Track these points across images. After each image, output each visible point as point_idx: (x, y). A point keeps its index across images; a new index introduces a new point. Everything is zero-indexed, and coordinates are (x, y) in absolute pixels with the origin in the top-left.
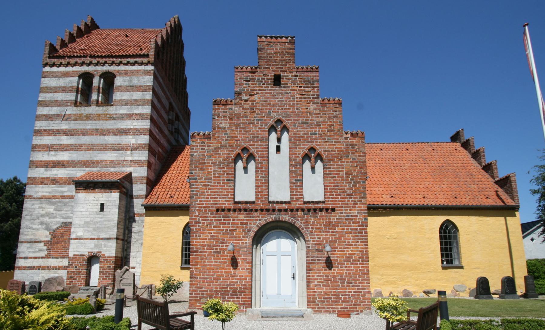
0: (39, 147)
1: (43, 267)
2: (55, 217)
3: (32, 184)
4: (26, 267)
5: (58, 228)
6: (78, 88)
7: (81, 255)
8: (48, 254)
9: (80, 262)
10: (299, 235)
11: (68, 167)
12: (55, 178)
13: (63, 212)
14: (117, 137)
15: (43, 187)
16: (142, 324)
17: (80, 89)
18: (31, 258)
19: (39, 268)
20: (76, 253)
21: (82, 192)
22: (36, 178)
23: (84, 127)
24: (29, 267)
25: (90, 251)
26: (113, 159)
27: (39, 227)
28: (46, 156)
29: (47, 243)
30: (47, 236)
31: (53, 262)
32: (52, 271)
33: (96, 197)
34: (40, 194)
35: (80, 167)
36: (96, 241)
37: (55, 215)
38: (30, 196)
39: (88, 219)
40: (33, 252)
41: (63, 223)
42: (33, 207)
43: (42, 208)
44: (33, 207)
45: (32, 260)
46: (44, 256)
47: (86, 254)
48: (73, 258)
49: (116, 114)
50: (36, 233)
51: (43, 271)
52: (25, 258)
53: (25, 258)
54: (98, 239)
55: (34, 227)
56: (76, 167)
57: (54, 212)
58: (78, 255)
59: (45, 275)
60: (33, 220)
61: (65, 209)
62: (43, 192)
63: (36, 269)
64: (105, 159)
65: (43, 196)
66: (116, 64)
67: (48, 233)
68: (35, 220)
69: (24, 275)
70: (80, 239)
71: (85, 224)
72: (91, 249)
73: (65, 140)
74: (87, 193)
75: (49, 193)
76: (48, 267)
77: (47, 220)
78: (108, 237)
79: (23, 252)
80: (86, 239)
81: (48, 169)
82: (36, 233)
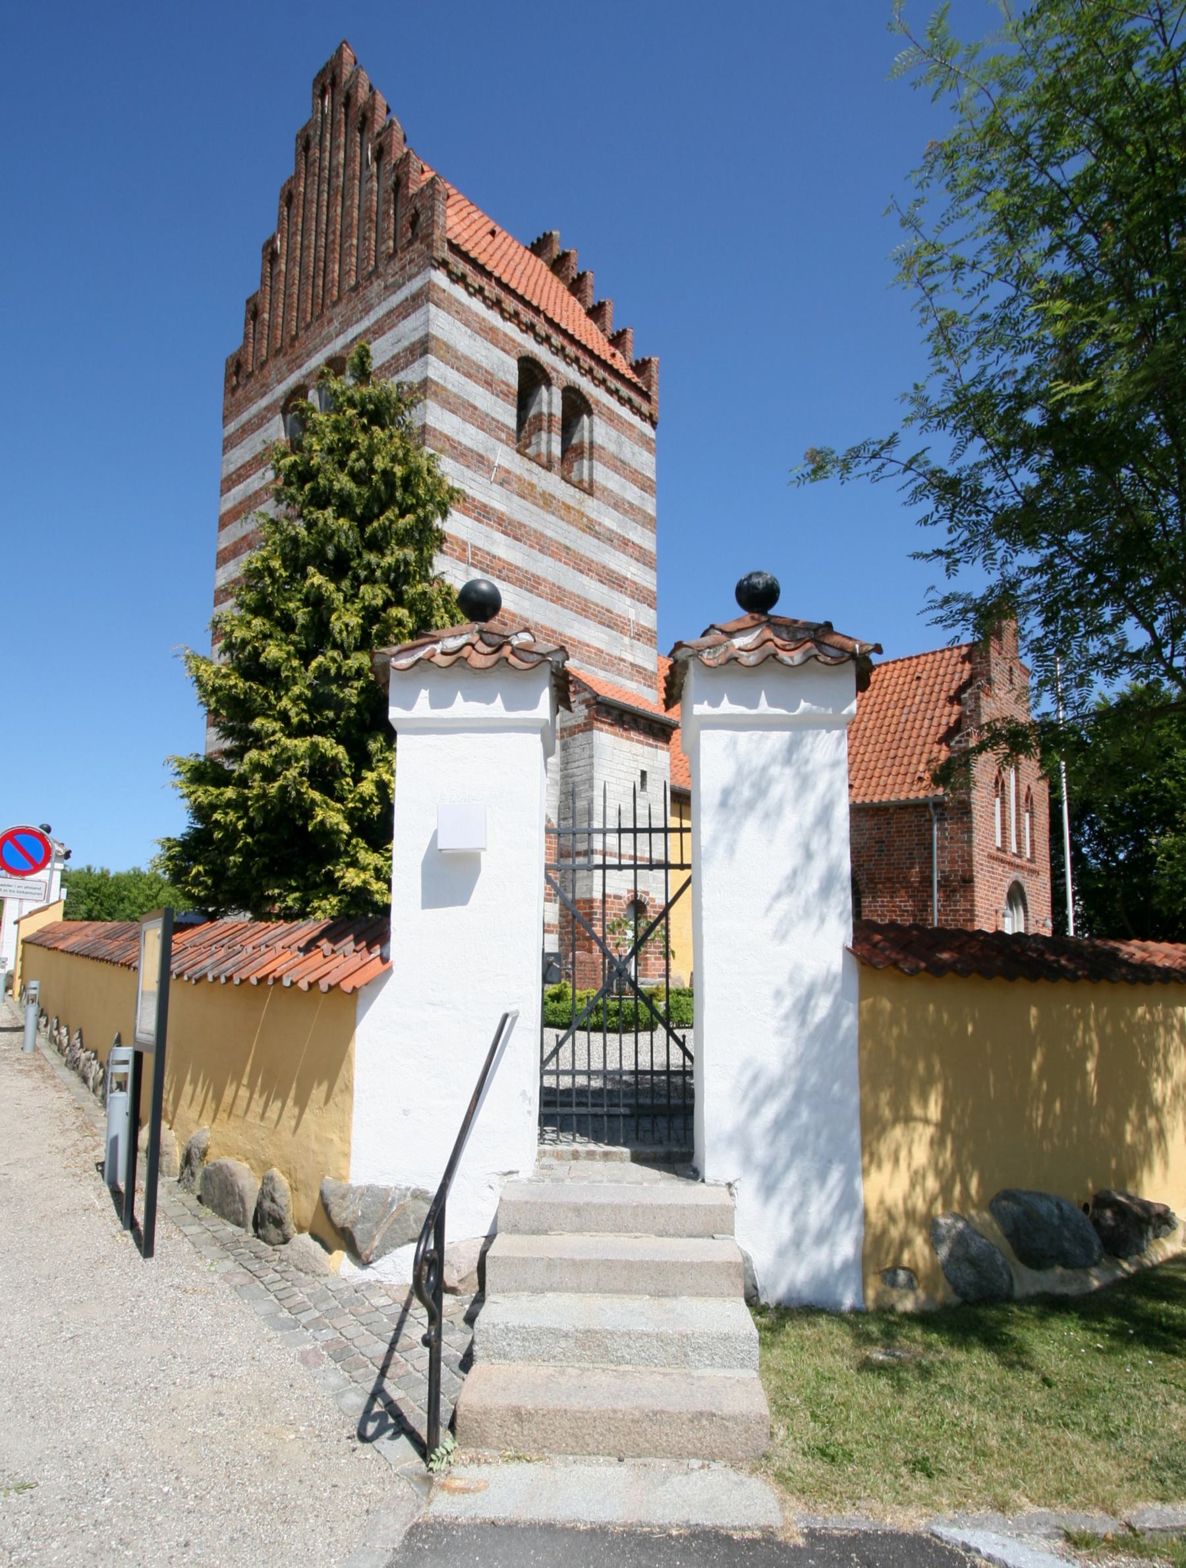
6: (591, 459)
10: (1020, 901)
17: (586, 455)
21: (607, 731)
23: (540, 528)
26: (602, 646)
49: (600, 524)
64: (587, 639)
66: (580, 367)
74: (616, 734)
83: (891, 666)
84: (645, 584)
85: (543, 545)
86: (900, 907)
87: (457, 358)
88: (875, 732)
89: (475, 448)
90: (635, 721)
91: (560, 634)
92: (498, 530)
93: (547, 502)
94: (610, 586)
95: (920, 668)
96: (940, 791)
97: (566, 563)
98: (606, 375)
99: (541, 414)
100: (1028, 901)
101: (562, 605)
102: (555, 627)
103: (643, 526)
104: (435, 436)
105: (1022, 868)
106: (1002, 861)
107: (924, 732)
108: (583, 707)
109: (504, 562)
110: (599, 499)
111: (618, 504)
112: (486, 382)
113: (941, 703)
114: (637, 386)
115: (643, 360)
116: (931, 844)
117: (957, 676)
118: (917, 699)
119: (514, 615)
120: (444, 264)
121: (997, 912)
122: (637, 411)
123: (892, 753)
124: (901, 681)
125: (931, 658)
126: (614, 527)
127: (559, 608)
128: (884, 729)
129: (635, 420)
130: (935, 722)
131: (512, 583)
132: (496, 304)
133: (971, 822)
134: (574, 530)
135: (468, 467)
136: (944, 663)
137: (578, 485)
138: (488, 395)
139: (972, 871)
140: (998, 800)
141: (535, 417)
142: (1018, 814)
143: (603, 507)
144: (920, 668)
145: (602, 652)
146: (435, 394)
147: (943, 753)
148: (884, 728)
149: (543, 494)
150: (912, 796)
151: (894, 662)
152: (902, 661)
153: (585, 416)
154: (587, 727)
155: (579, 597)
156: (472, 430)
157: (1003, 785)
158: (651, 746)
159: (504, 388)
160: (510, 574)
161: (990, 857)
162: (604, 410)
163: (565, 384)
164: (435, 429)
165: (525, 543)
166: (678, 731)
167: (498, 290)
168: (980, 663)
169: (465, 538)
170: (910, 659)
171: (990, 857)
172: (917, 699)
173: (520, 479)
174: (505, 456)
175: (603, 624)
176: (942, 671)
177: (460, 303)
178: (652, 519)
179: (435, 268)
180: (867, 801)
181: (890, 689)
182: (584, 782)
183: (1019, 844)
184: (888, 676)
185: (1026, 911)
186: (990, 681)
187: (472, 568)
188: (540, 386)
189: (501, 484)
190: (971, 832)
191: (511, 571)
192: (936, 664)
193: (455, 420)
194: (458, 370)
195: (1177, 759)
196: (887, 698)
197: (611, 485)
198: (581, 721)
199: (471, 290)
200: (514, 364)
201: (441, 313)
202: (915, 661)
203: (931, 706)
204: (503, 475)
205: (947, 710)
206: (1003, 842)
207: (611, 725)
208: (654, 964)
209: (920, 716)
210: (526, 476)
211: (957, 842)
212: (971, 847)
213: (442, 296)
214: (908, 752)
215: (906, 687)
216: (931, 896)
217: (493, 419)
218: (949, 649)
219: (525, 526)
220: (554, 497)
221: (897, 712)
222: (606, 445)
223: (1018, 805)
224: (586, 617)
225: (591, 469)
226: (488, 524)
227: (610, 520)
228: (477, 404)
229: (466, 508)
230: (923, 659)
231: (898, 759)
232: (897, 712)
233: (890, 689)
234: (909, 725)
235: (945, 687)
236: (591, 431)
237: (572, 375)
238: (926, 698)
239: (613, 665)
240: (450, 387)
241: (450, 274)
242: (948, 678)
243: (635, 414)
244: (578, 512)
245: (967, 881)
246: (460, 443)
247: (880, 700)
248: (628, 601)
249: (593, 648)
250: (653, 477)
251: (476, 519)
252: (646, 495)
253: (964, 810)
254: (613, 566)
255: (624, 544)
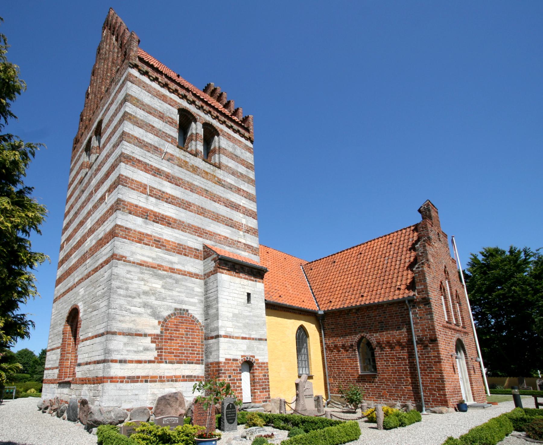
0: (132, 183)
1: (152, 377)
2: (164, 299)
3: (125, 238)
4: (124, 378)
5: (169, 316)
7: (234, 360)
8: (158, 355)
9: (234, 370)
11: (176, 228)
12: (159, 238)
13: (175, 293)
14: (228, 209)
15: (142, 248)
16: (538, 398)
17: (217, 152)
18: (131, 362)
19: (146, 379)
20: (229, 357)
21: (226, 274)
22: (131, 230)
23: (191, 181)
24: (129, 378)
25: (243, 354)
26: (227, 236)
27: (142, 310)
28: (143, 200)
29: (155, 339)
30: (154, 327)
31: (166, 369)
32: (167, 383)
33: (242, 283)
34: (139, 258)
35: (191, 234)
36: (247, 341)
37: (163, 296)
38: (123, 257)
39: (236, 312)
40: (135, 352)
41: (176, 309)
42: (128, 276)
43: (143, 280)
44: (128, 276)
45: (134, 365)
46: (153, 359)
47: (239, 358)
48: (225, 363)
49: (224, 181)
50: (138, 320)
51: (153, 384)
52: (121, 362)
53: (121, 362)
54: (249, 339)
55: (133, 309)
56: (186, 232)
57: (163, 291)
58: (230, 360)
59: (156, 391)
60: (130, 297)
61: (177, 289)
62: (143, 255)
63: (142, 381)
64: (219, 232)
65: (145, 262)
66: (212, 115)
67: (156, 322)
68: (134, 298)
69: (122, 393)
70: (230, 337)
71: (233, 317)
72: (244, 351)
73: (168, 188)
74: (231, 275)
75: (153, 259)
76: (161, 377)
77: (152, 300)
78: (259, 337)
79: (118, 351)
80: (237, 338)
81: (148, 221)
82: (138, 320)
83: (376, 241)
84: (251, 208)
85: (192, 188)
86: (396, 356)
87: (143, 105)
88: (372, 270)
89: (153, 144)
90: (242, 268)
91: (203, 229)
92: (166, 180)
93: (195, 170)
94: (231, 208)
95: (391, 239)
96: (412, 294)
97: (205, 197)
98: (226, 120)
99: (192, 134)
100: (466, 348)
101: (204, 216)
102: (200, 226)
103: (248, 183)
104: (129, 137)
105: (460, 331)
106: (450, 328)
107: (397, 267)
108: (213, 262)
109: (169, 195)
110: (224, 170)
111: (234, 173)
112: (160, 116)
113: (404, 253)
114: (243, 126)
115: (246, 117)
116: (410, 322)
117: (411, 240)
118: (392, 253)
119: (175, 219)
120: (135, 66)
121: (452, 356)
122: (243, 136)
123: (382, 278)
124: (382, 246)
125: (396, 234)
126: (233, 183)
127: (202, 217)
128: (376, 268)
129: (243, 140)
130: (403, 261)
131: (174, 205)
132: (165, 86)
133: (431, 309)
134: (210, 183)
135: (149, 151)
136: (403, 235)
137: (214, 165)
138: (161, 122)
139: (435, 334)
140: (442, 297)
141: (190, 136)
142: (453, 304)
143: (226, 174)
144: (391, 239)
145: (228, 238)
146: (130, 119)
147: (409, 275)
148: (376, 268)
149: (192, 166)
150: (395, 298)
151: (378, 239)
152: (382, 237)
153: (216, 137)
154: (215, 272)
155: (213, 212)
156: (151, 136)
157: (444, 290)
158: (253, 281)
159: (170, 120)
160: (173, 201)
161: (444, 326)
162: (226, 134)
163: (204, 121)
164: (129, 134)
165: (182, 187)
166: (268, 273)
167: (166, 80)
168: (422, 231)
169: (146, 183)
170: (385, 236)
171: (444, 326)
172: (392, 253)
173: (179, 159)
174: (171, 149)
175: (228, 225)
176: (402, 239)
177: (145, 83)
178: (253, 180)
179: (132, 68)
180: (372, 302)
181: (377, 250)
182: (214, 300)
183: (456, 319)
184: (375, 245)
185: (465, 354)
186: (429, 239)
187: (150, 197)
188: (191, 123)
189: (168, 160)
190: (432, 314)
191: (174, 199)
192: (399, 236)
193: (141, 131)
194: (143, 110)
195: (517, 278)
196: (376, 254)
197: (230, 165)
198: (212, 269)
199: (151, 78)
200: (176, 111)
201: (134, 86)
202: (388, 237)
203: (399, 254)
204: (169, 156)
205: (408, 256)
206: (448, 318)
207: (228, 270)
208: (259, 395)
209: (394, 260)
210: (182, 157)
211: (424, 320)
212: (433, 322)
213: (135, 79)
214: (390, 277)
215: (385, 248)
216: (414, 349)
217: (163, 132)
218: (404, 229)
219: (182, 180)
220: (199, 168)
221: (382, 259)
222: (227, 148)
223: (452, 299)
224: (218, 222)
225: (219, 158)
226: (159, 177)
227: (230, 180)
228: (154, 125)
229: (147, 170)
230: (392, 235)
231: (385, 281)
232: (382, 259)
233: (377, 250)
234: (389, 265)
235: (405, 245)
236: (219, 142)
237: (208, 118)
238: (396, 252)
239: (234, 244)
240: (138, 116)
241: (140, 71)
242: (406, 241)
243: (242, 137)
244: (212, 175)
245: (434, 340)
246: (144, 141)
247: (373, 255)
248: (242, 215)
249: (222, 236)
250: (253, 163)
251: (153, 175)
252: (249, 171)
253: (426, 301)
254: (232, 200)
255: (238, 190)
